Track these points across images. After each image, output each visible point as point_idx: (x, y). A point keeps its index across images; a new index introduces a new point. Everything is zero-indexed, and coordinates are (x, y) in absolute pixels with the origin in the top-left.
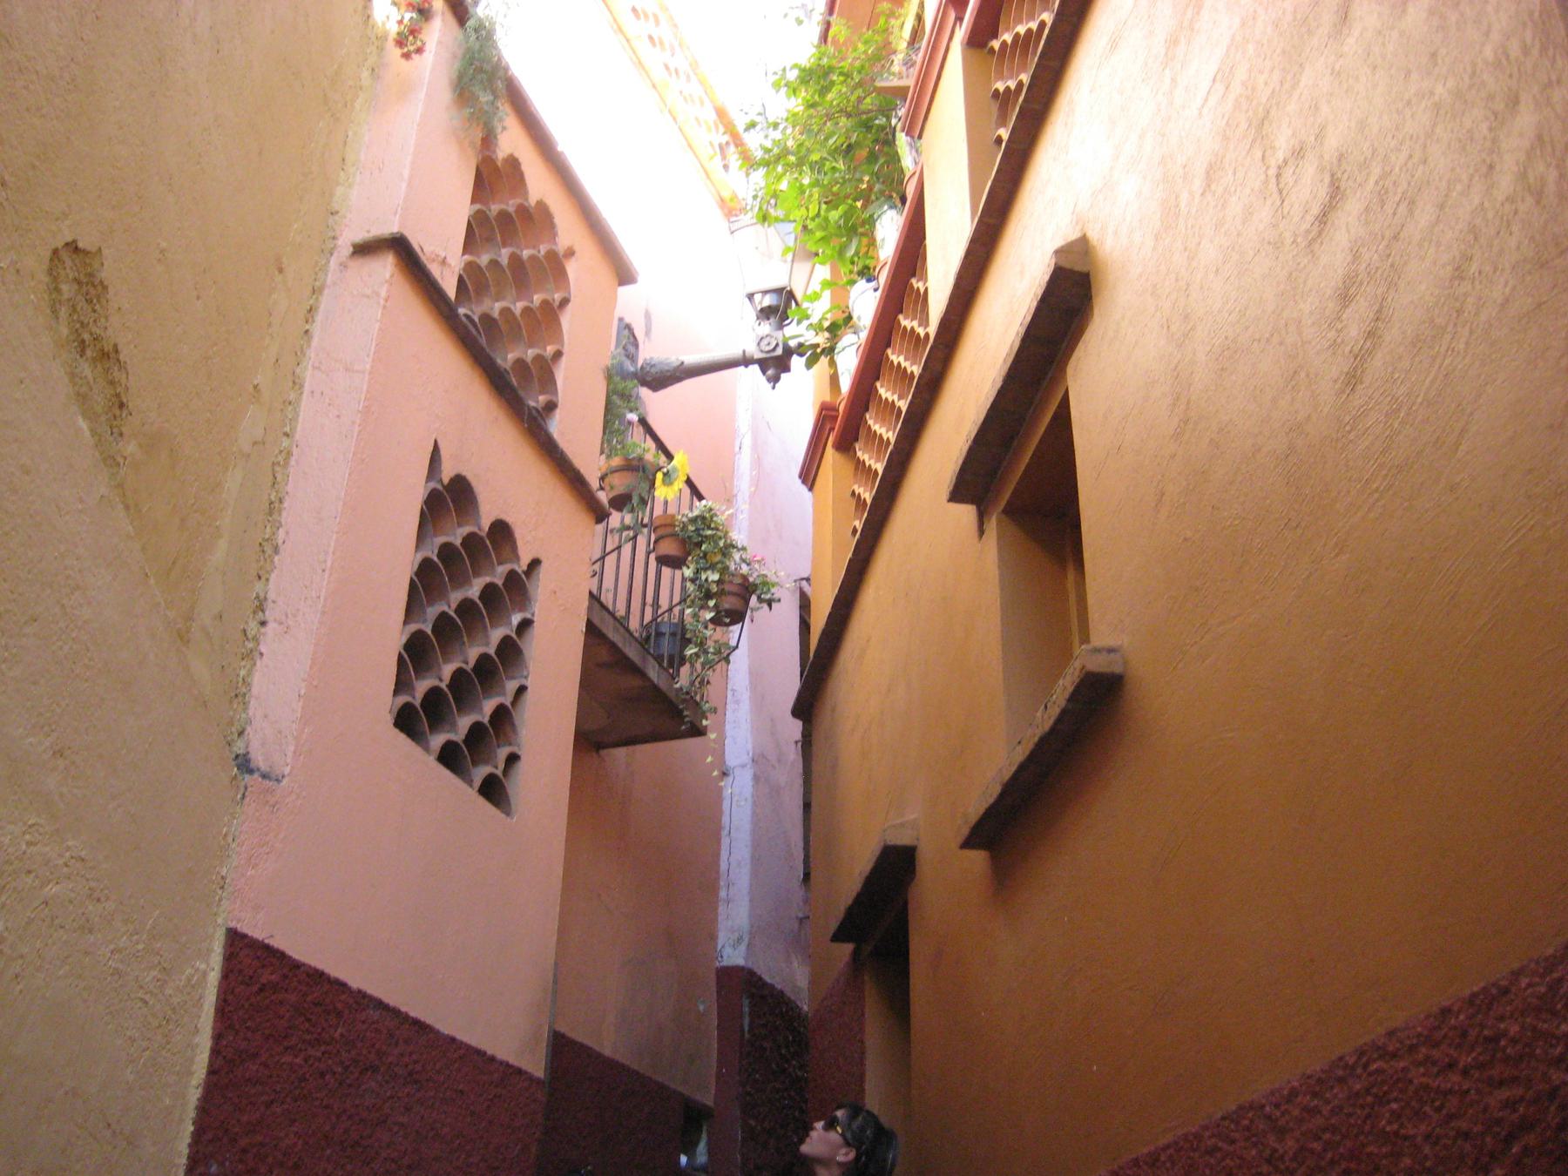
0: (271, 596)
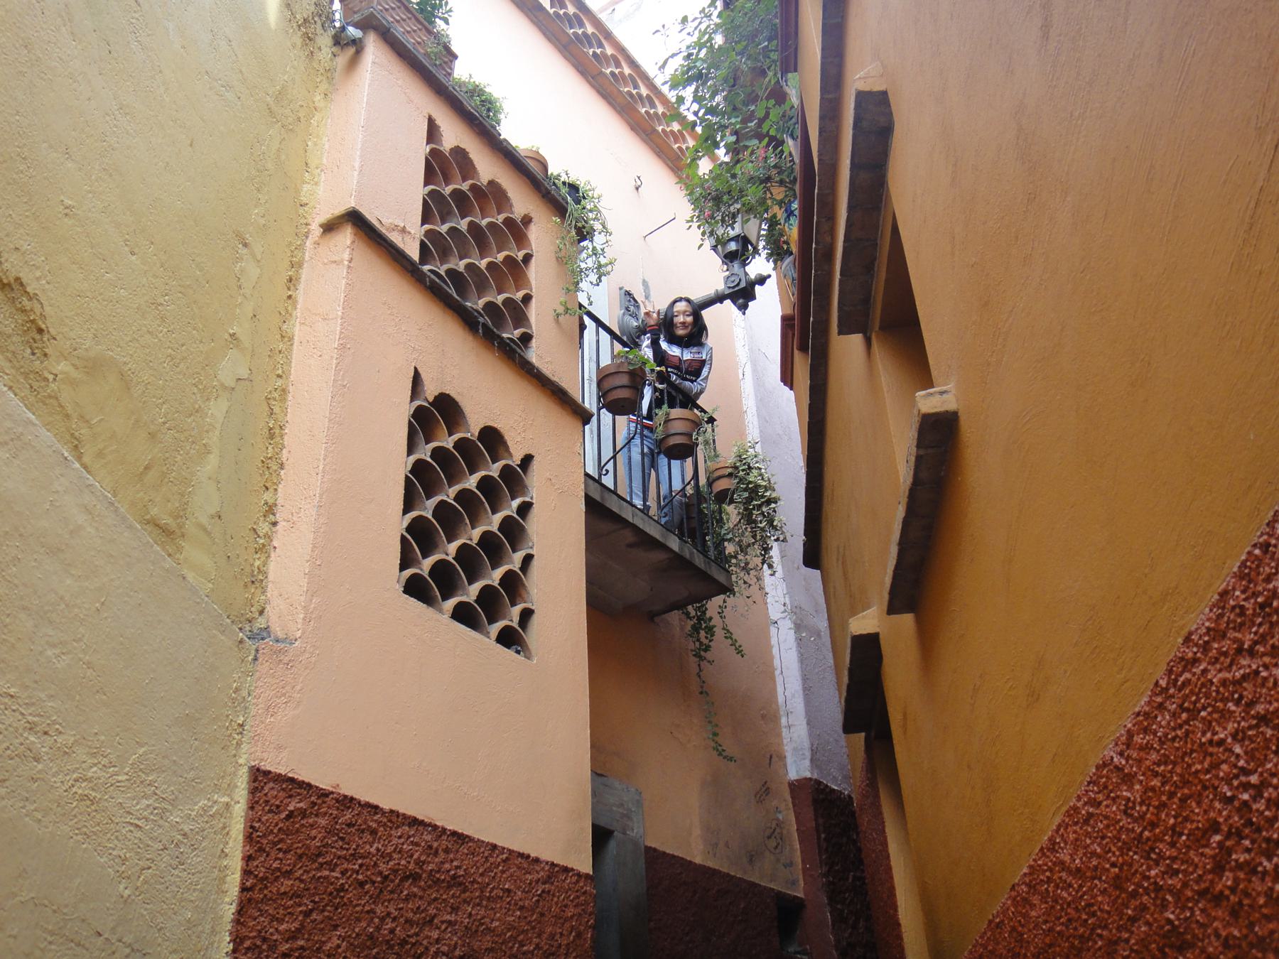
0: (280, 501)
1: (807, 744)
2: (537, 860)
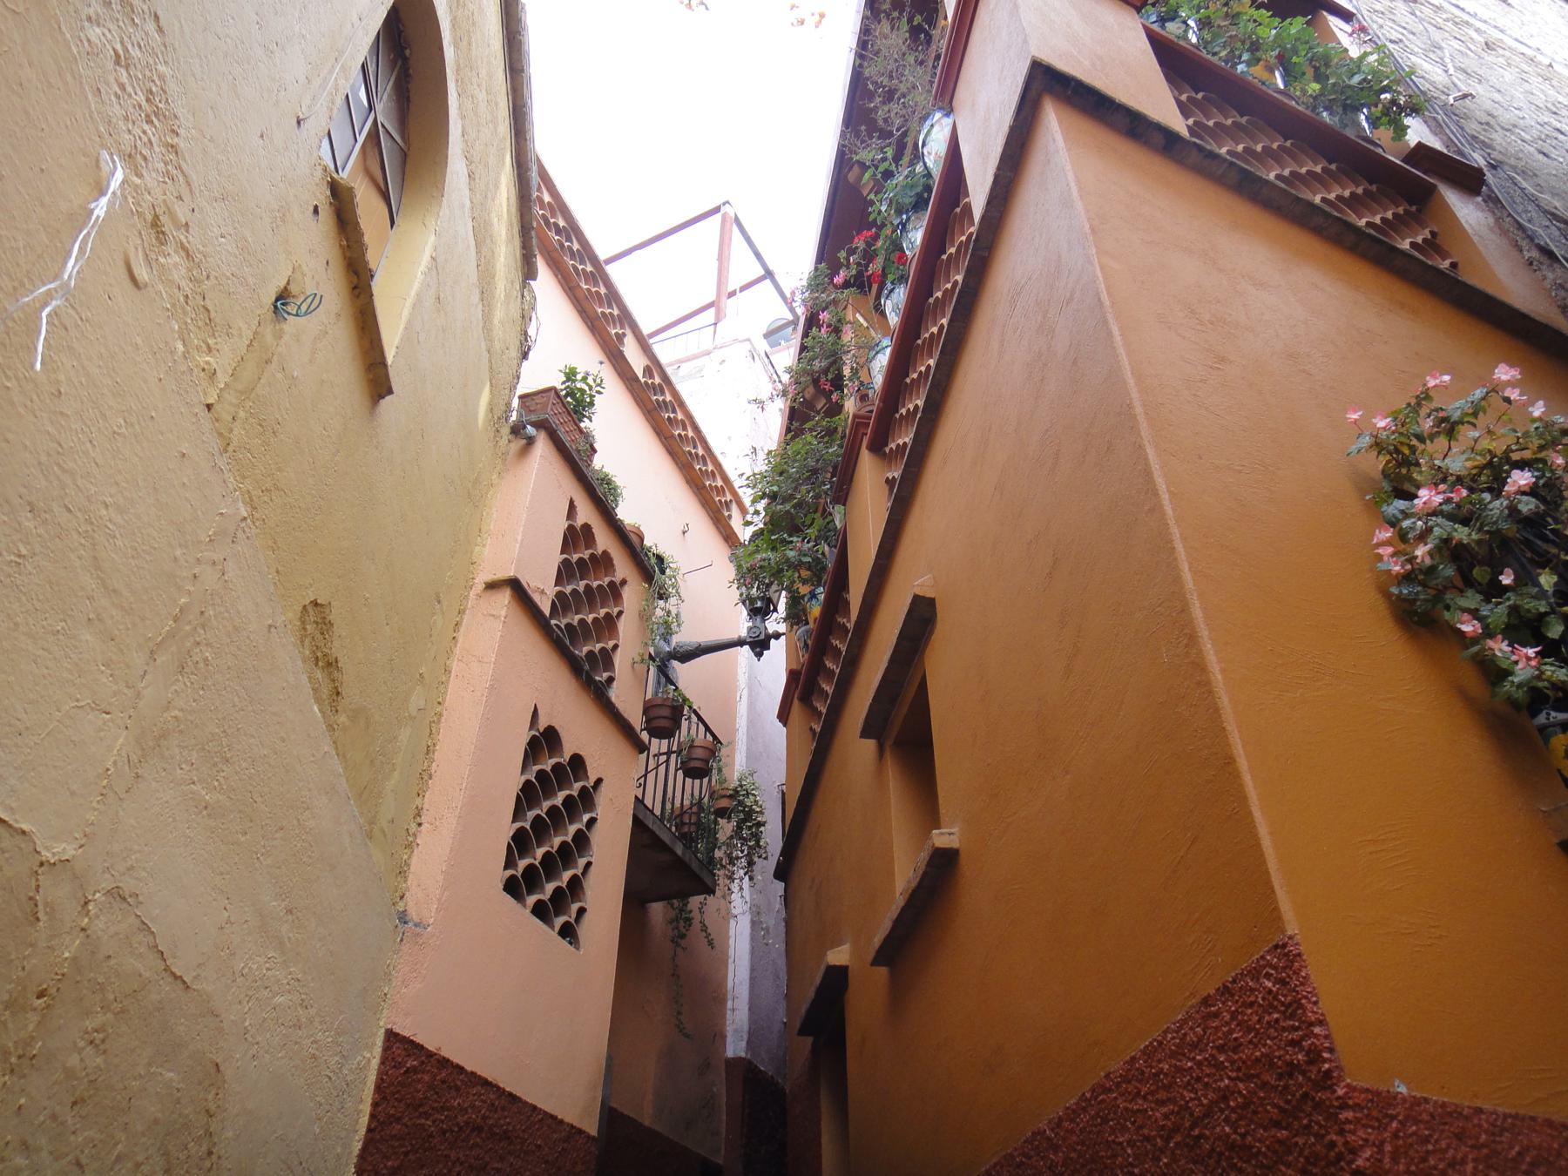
1: (746, 1028)
2: (561, 1122)
